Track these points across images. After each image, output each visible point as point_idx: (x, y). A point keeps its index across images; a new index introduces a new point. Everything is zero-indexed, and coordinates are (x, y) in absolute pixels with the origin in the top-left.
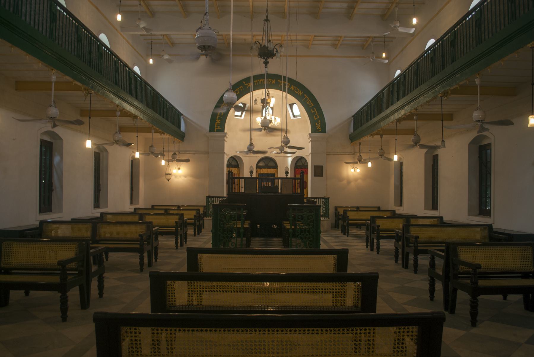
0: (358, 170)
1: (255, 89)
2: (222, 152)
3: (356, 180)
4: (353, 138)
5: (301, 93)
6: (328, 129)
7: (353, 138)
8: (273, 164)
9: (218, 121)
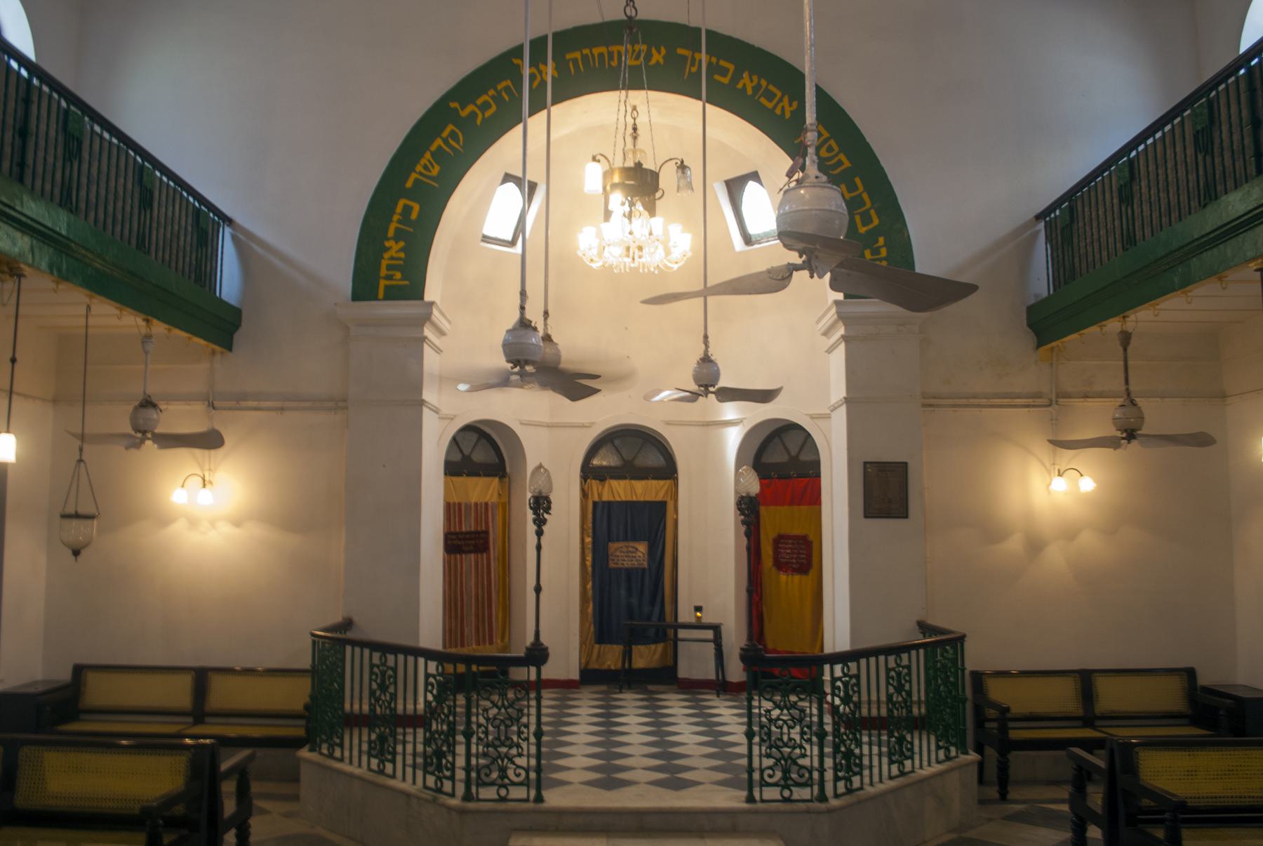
0: (1087, 485)
2: (410, 401)
3: (1069, 533)
4: (1046, 324)
7: (1046, 324)
8: (652, 459)
9: (394, 249)
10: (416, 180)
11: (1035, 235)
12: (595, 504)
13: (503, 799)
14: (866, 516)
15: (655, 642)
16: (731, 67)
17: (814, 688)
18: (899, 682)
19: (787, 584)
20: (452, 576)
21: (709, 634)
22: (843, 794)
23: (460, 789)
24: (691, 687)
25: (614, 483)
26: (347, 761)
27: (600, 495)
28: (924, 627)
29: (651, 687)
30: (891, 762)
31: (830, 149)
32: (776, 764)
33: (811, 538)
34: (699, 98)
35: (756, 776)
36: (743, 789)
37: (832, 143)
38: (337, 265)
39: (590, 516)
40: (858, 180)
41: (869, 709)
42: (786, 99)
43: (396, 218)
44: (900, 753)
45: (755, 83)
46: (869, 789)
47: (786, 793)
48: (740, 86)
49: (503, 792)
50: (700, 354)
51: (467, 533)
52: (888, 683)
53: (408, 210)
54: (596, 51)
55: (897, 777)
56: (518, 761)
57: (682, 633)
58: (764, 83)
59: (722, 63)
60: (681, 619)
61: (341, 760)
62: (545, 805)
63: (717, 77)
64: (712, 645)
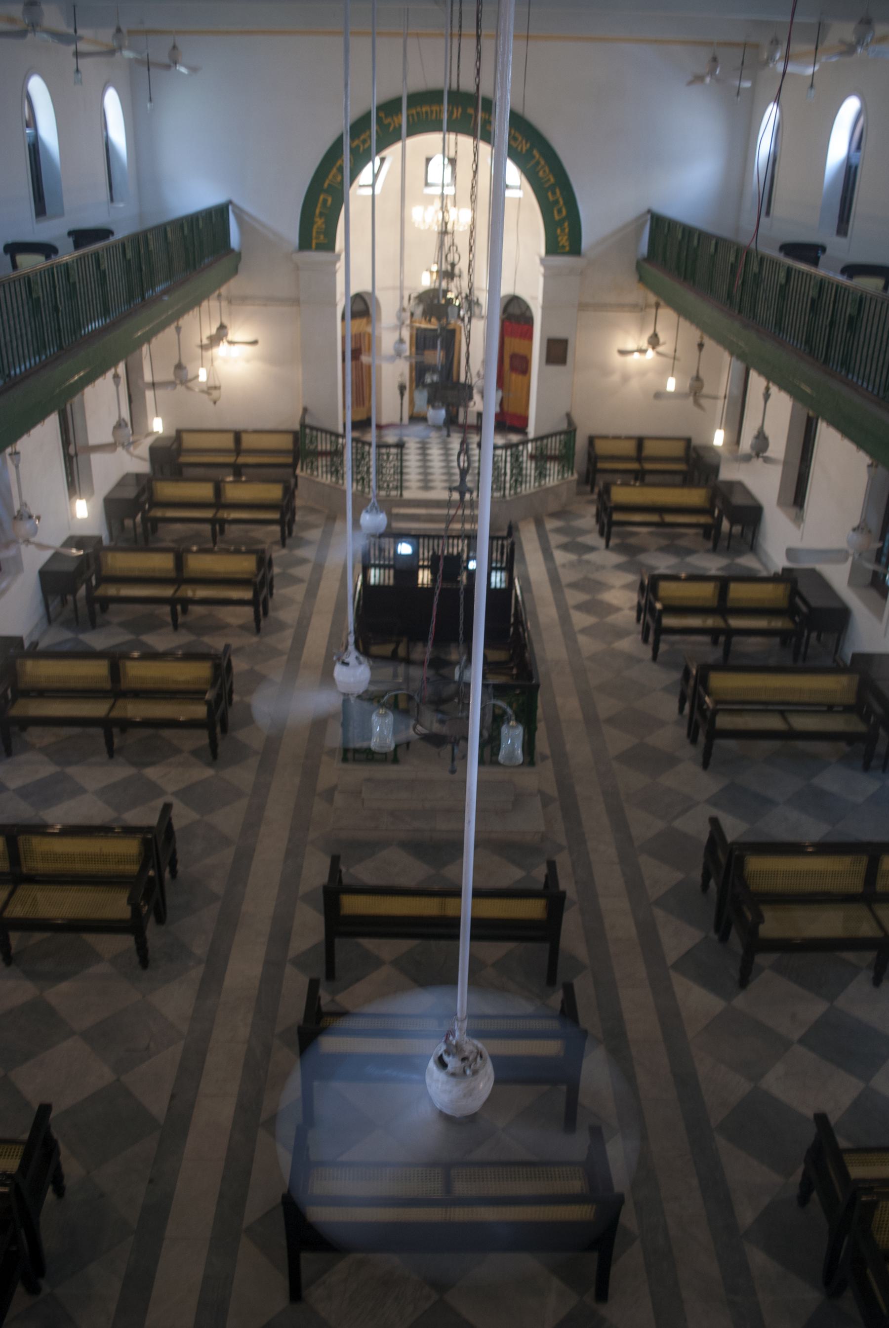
1: (411, 133)
6: (587, 240)
9: (319, 222)
11: (646, 221)
19: (514, 378)
38: (289, 228)
42: (524, 142)
53: (325, 201)
54: (424, 109)
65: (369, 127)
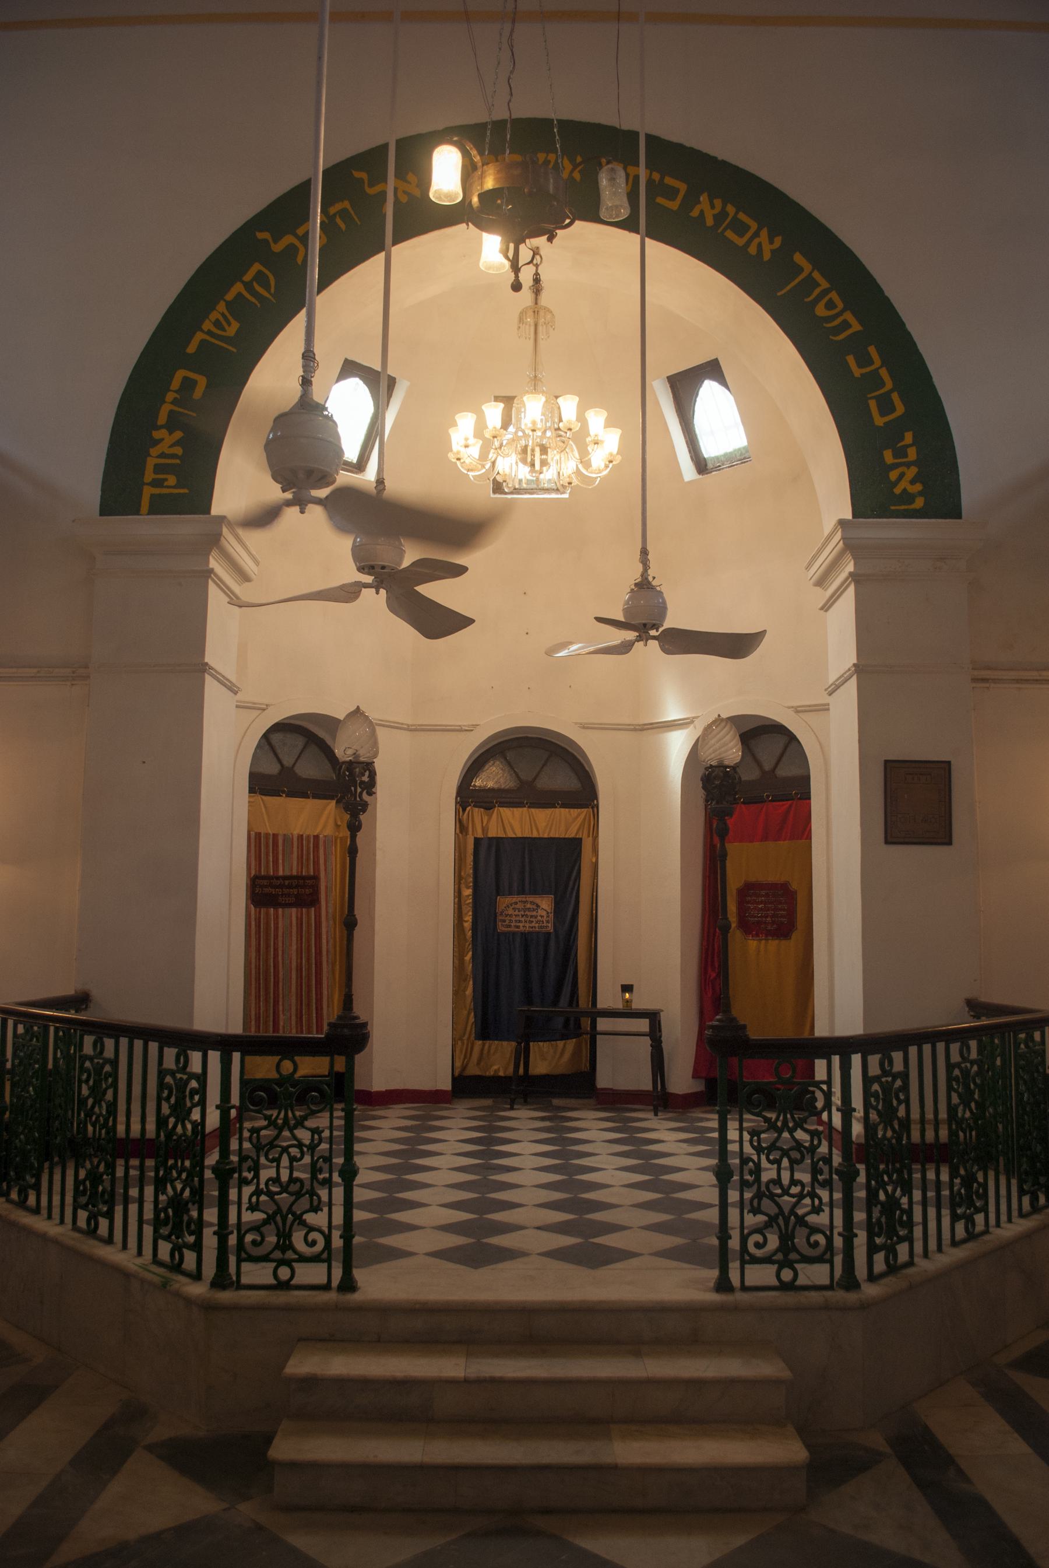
1: (397, 240)
2: (186, 664)
5: (766, 245)
6: (969, 496)
8: (560, 779)
9: (166, 442)
10: (203, 342)
12: (477, 841)
13: (284, 1286)
14: (887, 842)
15: (564, 1037)
16: (683, 187)
17: (798, 1101)
18: (887, 1102)
20: (260, 944)
21: (643, 1025)
22: (882, 1275)
23: (209, 1269)
24: (616, 1101)
25: (506, 812)
26: (44, 1212)
27: (485, 830)
28: (976, 1007)
29: (556, 1102)
30: (955, 1218)
31: (830, 305)
32: (768, 1225)
33: (794, 886)
34: (637, 232)
35: (734, 1243)
36: (705, 1264)
37: (834, 295)
39: (470, 859)
40: (872, 350)
41: (936, 1131)
42: (764, 233)
43: (170, 396)
44: (966, 1202)
45: (717, 211)
46: (921, 1263)
47: (787, 1275)
48: (695, 213)
49: (284, 1273)
50: (634, 573)
51: (285, 878)
52: (950, 1089)
53: (188, 385)
55: (964, 1241)
56: (310, 1218)
57: (603, 1024)
58: (731, 209)
59: (669, 181)
60: (601, 1004)
61: (36, 1211)
62: (357, 1297)
63: (660, 200)
64: (647, 1040)
65: (305, 216)
